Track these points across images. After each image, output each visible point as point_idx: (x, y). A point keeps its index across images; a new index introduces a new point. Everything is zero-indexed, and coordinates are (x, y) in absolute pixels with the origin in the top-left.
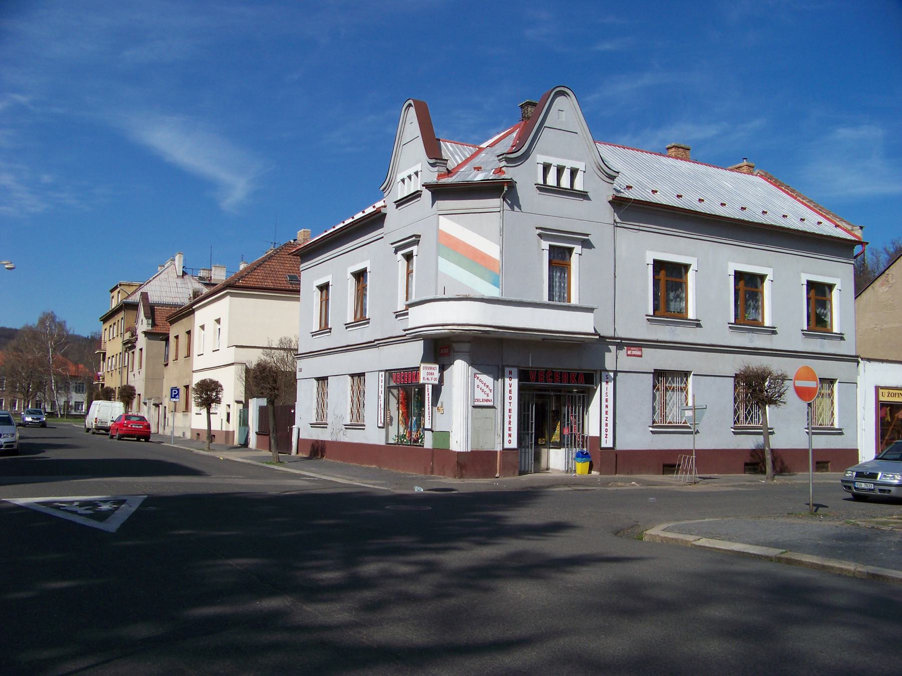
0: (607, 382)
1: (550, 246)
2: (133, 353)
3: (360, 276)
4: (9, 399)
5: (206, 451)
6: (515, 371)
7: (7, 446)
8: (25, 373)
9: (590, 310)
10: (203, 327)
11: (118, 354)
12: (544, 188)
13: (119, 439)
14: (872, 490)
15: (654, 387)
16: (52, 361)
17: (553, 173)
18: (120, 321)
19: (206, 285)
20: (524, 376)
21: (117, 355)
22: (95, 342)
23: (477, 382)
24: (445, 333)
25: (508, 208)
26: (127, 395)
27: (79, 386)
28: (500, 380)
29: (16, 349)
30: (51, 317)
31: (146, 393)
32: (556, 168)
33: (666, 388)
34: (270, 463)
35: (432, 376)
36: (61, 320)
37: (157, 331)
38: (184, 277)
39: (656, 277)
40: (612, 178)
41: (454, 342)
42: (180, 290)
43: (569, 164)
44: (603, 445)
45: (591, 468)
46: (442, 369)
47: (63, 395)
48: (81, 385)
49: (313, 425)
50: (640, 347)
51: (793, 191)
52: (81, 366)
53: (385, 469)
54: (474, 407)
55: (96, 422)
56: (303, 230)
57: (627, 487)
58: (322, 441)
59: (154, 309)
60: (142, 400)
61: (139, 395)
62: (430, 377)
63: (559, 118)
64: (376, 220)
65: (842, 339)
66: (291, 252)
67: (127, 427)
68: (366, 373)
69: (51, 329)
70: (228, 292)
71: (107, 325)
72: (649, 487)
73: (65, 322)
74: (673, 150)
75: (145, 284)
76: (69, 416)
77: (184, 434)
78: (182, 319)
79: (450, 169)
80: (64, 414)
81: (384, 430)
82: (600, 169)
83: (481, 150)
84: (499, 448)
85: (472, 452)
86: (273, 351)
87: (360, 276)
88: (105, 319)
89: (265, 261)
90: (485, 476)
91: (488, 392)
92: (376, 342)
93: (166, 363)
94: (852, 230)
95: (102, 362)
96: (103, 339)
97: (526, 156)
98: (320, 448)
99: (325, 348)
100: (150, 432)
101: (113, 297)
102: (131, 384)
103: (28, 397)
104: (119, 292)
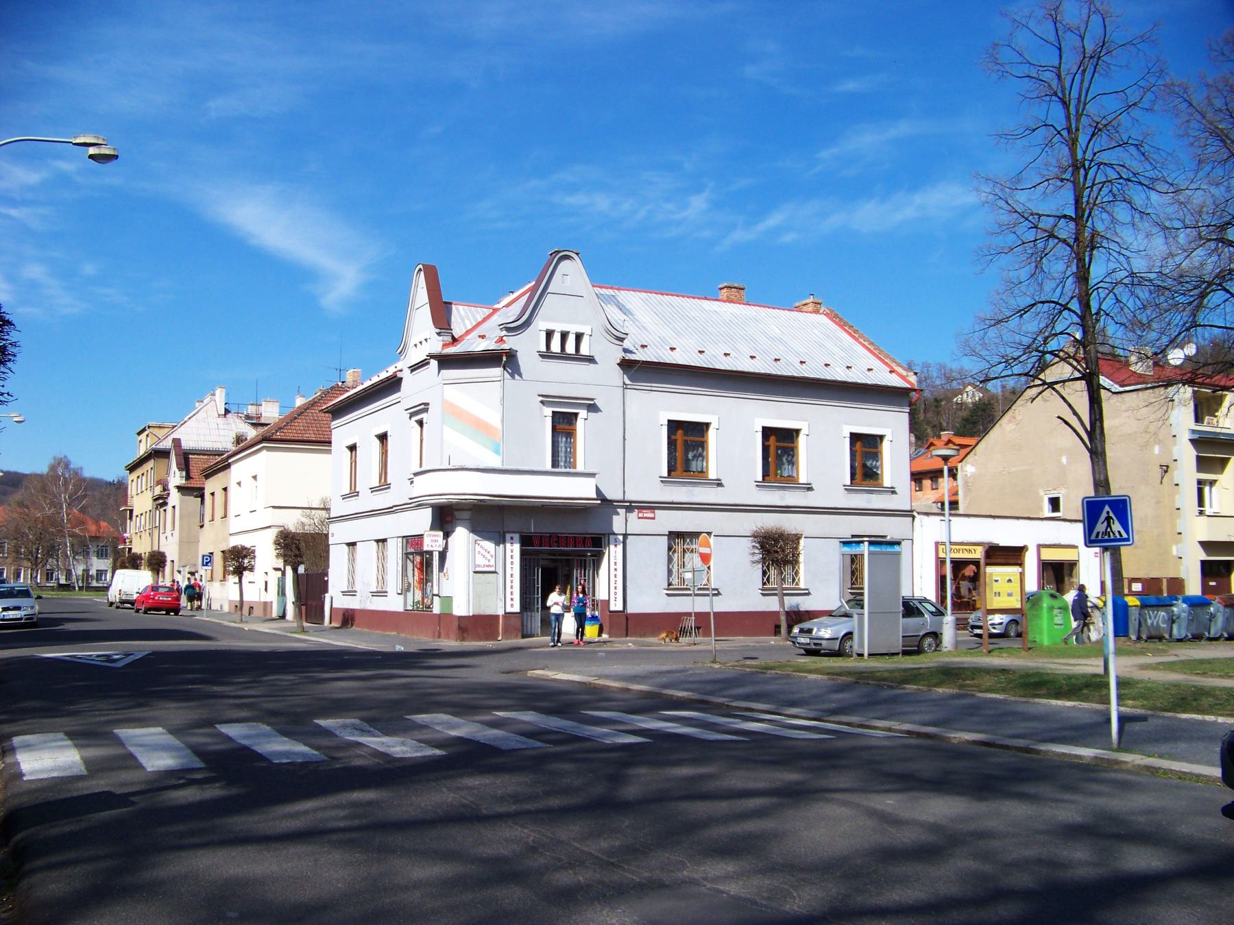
0: (616, 546)
1: (553, 412)
2: (165, 510)
3: (383, 438)
4: (13, 568)
5: (239, 623)
6: (517, 536)
7: (26, 619)
8: (34, 535)
9: (593, 475)
10: (239, 484)
11: (148, 512)
12: (547, 355)
13: (145, 613)
14: (809, 644)
15: (670, 549)
16: (67, 520)
17: (556, 340)
18: (149, 471)
19: (255, 425)
20: (525, 541)
21: (146, 512)
22: (120, 489)
23: (477, 548)
24: (443, 503)
25: (509, 377)
26: (157, 562)
27: (102, 550)
28: (501, 545)
29: (21, 504)
30: (63, 463)
31: (180, 559)
32: (560, 334)
33: (684, 550)
34: (294, 633)
35: (435, 543)
36: (76, 466)
37: (192, 486)
38: (227, 416)
39: (673, 437)
40: (622, 340)
41: (457, 510)
42: (222, 432)
43: (573, 329)
44: (612, 608)
45: (600, 633)
46: (447, 535)
47: (80, 562)
48: (104, 548)
49: (344, 593)
50: (653, 509)
51: (856, 331)
52: (104, 524)
53: (403, 635)
54: (475, 572)
55: (120, 594)
56: (352, 370)
57: (624, 647)
58: (352, 609)
59: (189, 458)
60: (176, 568)
61: (173, 561)
62: (434, 544)
63: (563, 283)
64: (392, 385)
65: (894, 492)
66: (320, 408)
67: (153, 599)
68: (358, 543)
69: (64, 478)
70: (263, 447)
71: (134, 476)
72: (643, 648)
73: (81, 469)
74: (725, 290)
75: (179, 425)
76: (89, 588)
77: (221, 606)
78: (217, 473)
79: (456, 337)
80: (83, 587)
81: (402, 596)
82: (608, 331)
83: (495, 310)
84: (501, 612)
85: (473, 616)
86: (313, 511)
87: (383, 438)
88: (132, 468)
89: (308, 408)
90: (487, 639)
91: (489, 557)
92: (395, 508)
93: (201, 524)
94: (907, 376)
95: (128, 521)
96: (129, 493)
97: (527, 324)
98: (350, 618)
99: (353, 513)
100: (180, 604)
101: (140, 441)
102: (162, 550)
103: (36, 565)
104: (147, 436)
